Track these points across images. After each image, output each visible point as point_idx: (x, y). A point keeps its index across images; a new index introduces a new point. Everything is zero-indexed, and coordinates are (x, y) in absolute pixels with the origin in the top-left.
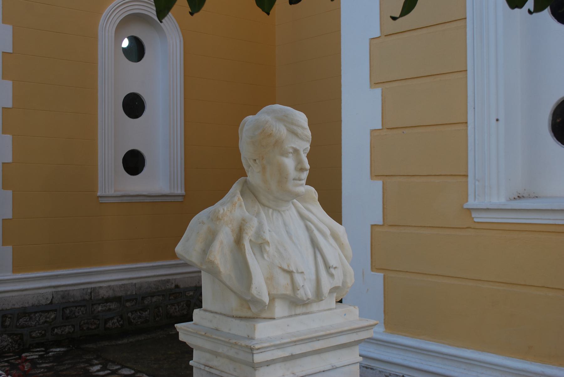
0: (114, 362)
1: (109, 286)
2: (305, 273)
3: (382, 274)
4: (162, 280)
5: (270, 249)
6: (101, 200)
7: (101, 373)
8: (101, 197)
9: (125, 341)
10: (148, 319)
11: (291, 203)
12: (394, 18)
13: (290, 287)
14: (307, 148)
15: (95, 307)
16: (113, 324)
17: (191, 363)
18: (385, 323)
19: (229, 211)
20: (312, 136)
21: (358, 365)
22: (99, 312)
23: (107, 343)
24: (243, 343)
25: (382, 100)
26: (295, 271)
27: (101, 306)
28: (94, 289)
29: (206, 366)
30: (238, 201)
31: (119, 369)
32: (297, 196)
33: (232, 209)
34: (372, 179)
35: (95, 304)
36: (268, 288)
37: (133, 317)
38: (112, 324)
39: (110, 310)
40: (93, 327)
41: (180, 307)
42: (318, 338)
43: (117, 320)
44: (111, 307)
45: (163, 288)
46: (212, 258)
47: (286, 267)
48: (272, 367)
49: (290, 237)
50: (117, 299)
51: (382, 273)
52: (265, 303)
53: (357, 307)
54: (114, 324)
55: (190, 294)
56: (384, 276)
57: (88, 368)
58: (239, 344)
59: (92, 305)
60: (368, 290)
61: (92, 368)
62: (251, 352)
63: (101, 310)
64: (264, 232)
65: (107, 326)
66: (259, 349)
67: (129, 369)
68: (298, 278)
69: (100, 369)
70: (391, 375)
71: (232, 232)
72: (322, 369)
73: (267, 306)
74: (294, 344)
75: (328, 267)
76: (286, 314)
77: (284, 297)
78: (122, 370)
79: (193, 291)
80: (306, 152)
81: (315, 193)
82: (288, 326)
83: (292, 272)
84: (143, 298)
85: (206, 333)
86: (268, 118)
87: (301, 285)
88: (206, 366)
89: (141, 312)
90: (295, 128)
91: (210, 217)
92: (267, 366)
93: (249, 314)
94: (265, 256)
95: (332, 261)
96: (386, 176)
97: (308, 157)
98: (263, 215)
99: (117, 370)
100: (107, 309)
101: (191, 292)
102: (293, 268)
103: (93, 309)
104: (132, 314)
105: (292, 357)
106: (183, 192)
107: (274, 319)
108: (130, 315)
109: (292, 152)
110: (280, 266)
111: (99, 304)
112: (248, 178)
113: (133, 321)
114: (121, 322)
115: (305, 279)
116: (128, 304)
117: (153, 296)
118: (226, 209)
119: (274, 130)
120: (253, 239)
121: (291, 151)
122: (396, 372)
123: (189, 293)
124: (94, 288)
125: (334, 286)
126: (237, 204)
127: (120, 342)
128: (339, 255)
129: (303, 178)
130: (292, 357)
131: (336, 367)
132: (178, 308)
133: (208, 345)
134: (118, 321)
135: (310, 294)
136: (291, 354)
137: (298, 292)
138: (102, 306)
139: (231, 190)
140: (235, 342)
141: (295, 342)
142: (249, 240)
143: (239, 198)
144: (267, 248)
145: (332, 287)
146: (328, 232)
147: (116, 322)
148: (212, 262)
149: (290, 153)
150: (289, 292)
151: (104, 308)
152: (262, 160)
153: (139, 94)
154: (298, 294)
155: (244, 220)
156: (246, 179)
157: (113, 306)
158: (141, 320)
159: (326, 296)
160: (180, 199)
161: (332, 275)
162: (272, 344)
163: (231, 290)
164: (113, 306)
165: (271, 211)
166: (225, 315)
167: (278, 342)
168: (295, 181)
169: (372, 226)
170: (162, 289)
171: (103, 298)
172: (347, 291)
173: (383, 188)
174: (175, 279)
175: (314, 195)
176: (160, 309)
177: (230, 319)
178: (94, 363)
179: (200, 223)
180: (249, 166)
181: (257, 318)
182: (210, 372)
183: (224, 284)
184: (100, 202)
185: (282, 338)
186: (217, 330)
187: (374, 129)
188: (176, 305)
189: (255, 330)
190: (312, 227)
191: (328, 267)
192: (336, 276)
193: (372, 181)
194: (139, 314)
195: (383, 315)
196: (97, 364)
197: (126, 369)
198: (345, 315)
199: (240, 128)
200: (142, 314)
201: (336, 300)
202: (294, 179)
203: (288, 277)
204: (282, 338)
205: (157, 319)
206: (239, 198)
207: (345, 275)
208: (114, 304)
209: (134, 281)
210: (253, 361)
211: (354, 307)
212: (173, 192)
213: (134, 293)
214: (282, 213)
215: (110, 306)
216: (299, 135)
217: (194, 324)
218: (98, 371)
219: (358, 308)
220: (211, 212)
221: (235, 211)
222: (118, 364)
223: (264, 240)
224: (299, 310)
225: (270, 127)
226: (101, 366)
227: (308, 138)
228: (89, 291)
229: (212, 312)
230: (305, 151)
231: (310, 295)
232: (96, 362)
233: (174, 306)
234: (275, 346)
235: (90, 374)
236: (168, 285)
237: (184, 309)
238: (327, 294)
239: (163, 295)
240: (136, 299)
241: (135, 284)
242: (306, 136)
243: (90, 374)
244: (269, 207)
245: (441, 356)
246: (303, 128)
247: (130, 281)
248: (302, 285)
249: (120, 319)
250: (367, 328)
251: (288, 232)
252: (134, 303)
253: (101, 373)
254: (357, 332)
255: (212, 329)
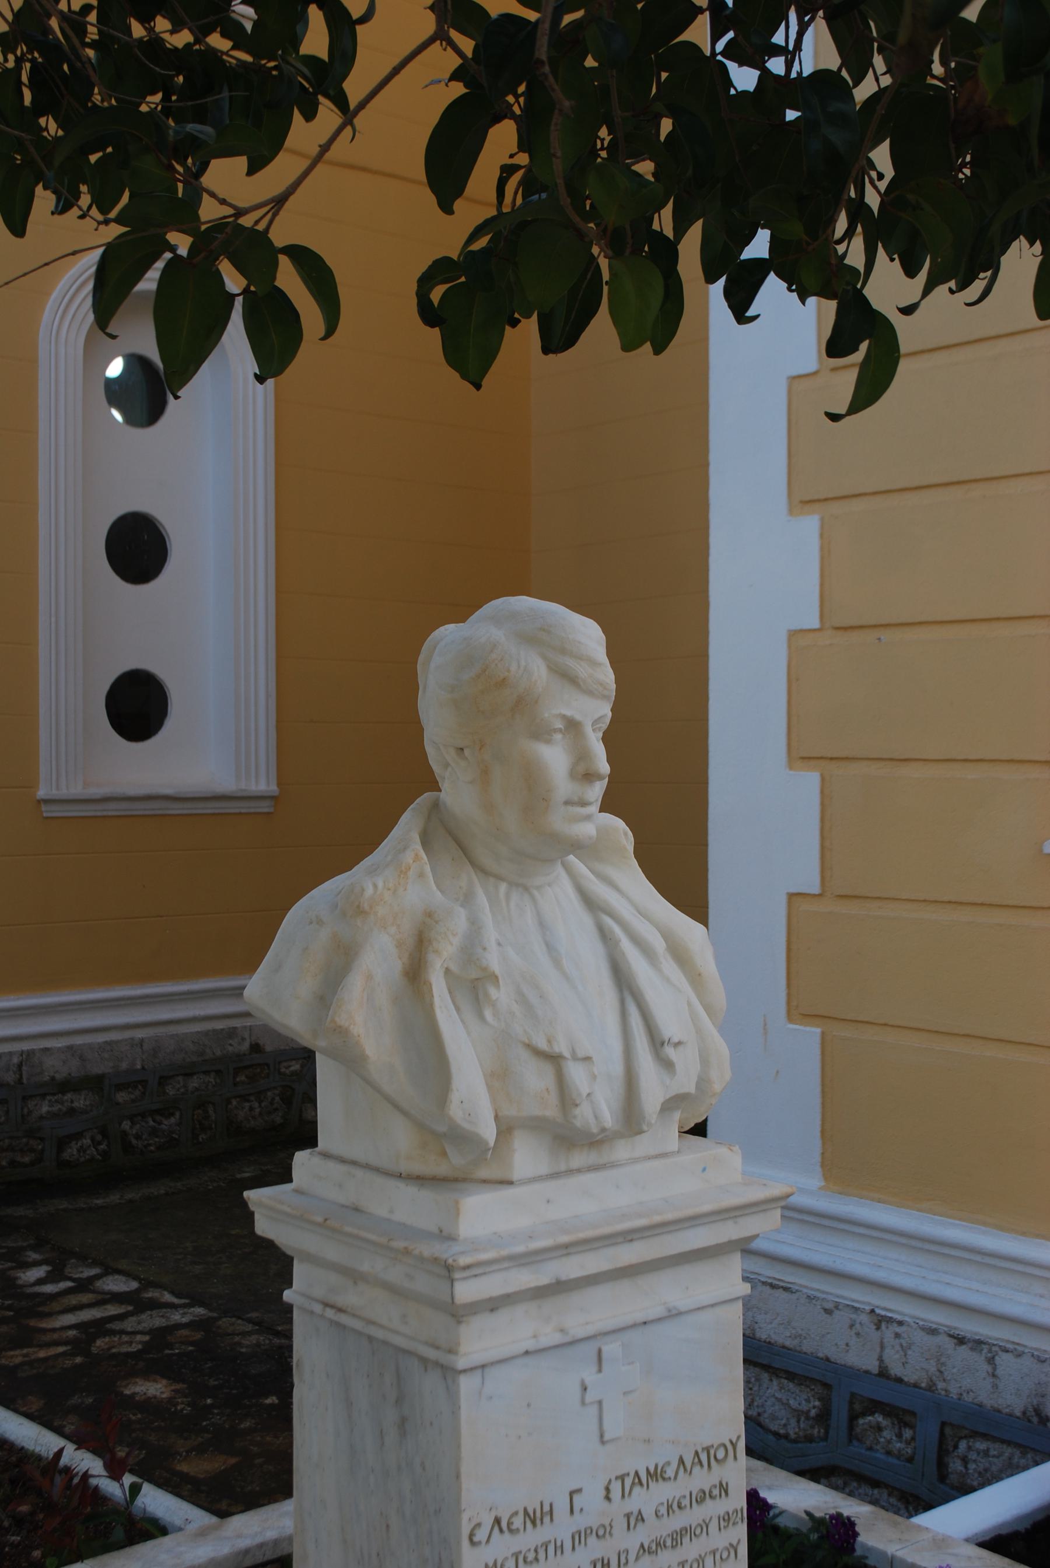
0: (84, 1259)
1: (70, 1048)
2: (594, 1059)
3: (818, 1030)
4: (214, 1031)
5: (502, 995)
6: (47, 811)
7: (49, 1288)
8: (46, 801)
9: (114, 1198)
10: (177, 1137)
11: (560, 862)
12: (834, 417)
13: (553, 1099)
14: (604, 716)
15: (31, 1104)
16: (82, 1150)
17: (288, 1295)
18: (823, 1165)
19: (389, 889)
20: (616, 683)
21: (740, 1304)
22: (41, 1118)
23: (64, 1205)
24: (428, 1249)
25: (822, 549)
26: (566, 1054)
27: (47, 1102)
28: (30, 1053)
29: (326, 1305)
30: (414, 862)
31: (98, 1277)
32: (576, 846)
33: (399, 884)
34: (791, 768)
35: (31, 1097)
36: (494, 1100)
37: (134, 1132)
38: (79, 1151)
39: (72, 1112)
40: (27, 1159)
41: (263, 1104)
42: (629, 1236)
43: (93, 1139)
44: (76, 1104)
45: (218, 1053)
46: (342, 1020)
47: (542, 1044)
48: (503, 1316)
49: (557, 963)
50: (94, 1083)
51: (817, 1026)
52: (487, 1143)
53: (737, 1147)
54: (85, 1151)
55: (292, 1068)
56: (823, 1033)
57: (12, 1273)
58: (416, 1252)
59: (25, 1098)
60: (778, 1072)
61: (24, 1273)
62: (447, 1274)
63: (48, 1112)
64: (485, 949)
65: (66, 1155)
66: (468, 1267)
67: (124, 1279)
68: (576, 1074)
69: (46, 1277)
70: (840, 1307)
71: (397, 947)
72: (640, 1317)
73: (491, 1151)
74: (565, 1252)
75: (657, 1043)
76: (544, 1169)
77: (537, 1125)
78: (104, 1279)
79: (300, 1062)
80: (601, 727)
81: (626, 834)
82: (548, 1202)
83: (558, 1057)
84: (163, 1080)
85: (326, 1220)
86: (498, 634)
87: (584, 1090)
88: (326, 1305)
89: (158, 1118)
90: (571, 663)
91: (337, 906)
92: (492, 1310)
93: (442, 1169)
94: (488, 1014)
95: (671, 1026)
96: (831, 759)
97: (606, 739)
98: (481, 898)
99: (92, 1279)
100: (64, 1109)
101: (294, 1062)
102: (561, 1047)
103: (26, 1111)
104: (133, 1123)
105: (559, 1288)
106: (273, 788)
107: (510, 1183)
108: (126, 1125)
109: (563, 728)
110: (527, 1041)
111: (43, 1096)
112: (442, 795)
113: (134, 1142)
114: (103, 1147)
115: (594, 1077)
116: (122, 1097)
117: (189, 1075)
118: (380, 884)
119: (513, 668)
120: (453, 967)
121: (559, 725)
122: (853, 1301)
123: (290, 1066)
124: (28, 1050)
125: (674, 1094)
126: (411, 870)
127: (99, 1202)
128: (689, 1004)
129: (592, 800)
130: (559, 1288)
131: (677, 1312)
132: (260, 1106)
133: (332, 1252)
134: (95, 1143)
135: (610, 1120)
136: (557, 1279)
137: (577, 1111)
138: (50, 1101)
139: (396, 832)
140: (406, 1248)
141: (567, 1248)
142: (444, 969)
143: (417, 855)
144: (493, 992)
145: (668, 1097)
146: (659, 944)
147: (90, 1146)
148: (342, 1032)
149: (555, 731)
150: (551, 1111)
151: (56, 1108)
152: (480, 749)
153: (153, 517)
154: (575, 1117)
155: (429, 914)
156: (438, 799)
157: (80, 1101)
158: (157, 1140)
159: (653, 1122)
160: (265, 807)
161: (668, 1065)
162: (504, 1253)
163: (396, 1106)
164: (82, 1102)
165: (503, 887)
166: (377, 1170)
167: (520, 1249)
168: (570, 808)
169: (791, 896)
170: (214, 1053)
171: (53, 1079)
172: (711, 1104)
173: (822, 792)
174: (250, 1026)
175: (624, 842)
176: (211, 1110)
177: (392, 1183)
178: (30, 1260)
179: (311, 923)
180: (447, 765)
181: (464, 1180)
182: (338, 1324)
183: (377, 1090)
184: (45, 815)
185: (530, 1237)
186: (357, 1209)
187: (799, 628)
188: (252, 1098)
189: (458, 1214)
190: (617, 930)
191: (657, 1043)
192: (679, 1067)
193: (792, 772)
194: (151, 1123)
195: (818, 1142)
196: (36, 1264)
197: (116, 1277)
198: (704, 1170)
199: (421, 658)
200: (160, 1123)
201: (680, 1127)
202: (567, 803)
203: (548, 1069)
204: (530, 1237)
205: (201, 1139)
206: (417, 855)
207: (705, 1061)
208: (83, 1098)
209: (139, 1034)
210: (453, 1298)
211: (731, 1150)
212: (244, 787)
213: (139, 1067)
214: (536, 893)
215: (72, 1102)
216: (581, 683)
217: (297, 1191)
218: (40, 1282)
219: (740, 1151)
220: (340, 892)
221: (405, 890)
222: (95, 1263)
223: (485, 969)
224: (579, 1159)
225: (502, 660)
226: (49, 1268)
227: (605, 688)
228: (16, 1060)
229: (343, 1161)
230: (598, 726)
231: (609, 1119)
232: (34, 1256)
233: (248, 1101)
234: (511, 1258)
235: (19, 1290)
236: (231, 1045)
237: (276, 1109)
238: (655, 1116)
239: (218, 1072)
240: (144, 1083)
241: (142, 1041)
242: (601, 684)
243: (19, 1290)
244: (500, 878)
245: (978, 1258)
246: (594, 663)
247: (127, 1034)
248: (587, 1091)
249: (99, 1137)
250: (764, 1207)
251: (550, 948)
252: (137, 1093)
253: (49, 1288)
254: (736, 1217)
255: (343, 1206)
